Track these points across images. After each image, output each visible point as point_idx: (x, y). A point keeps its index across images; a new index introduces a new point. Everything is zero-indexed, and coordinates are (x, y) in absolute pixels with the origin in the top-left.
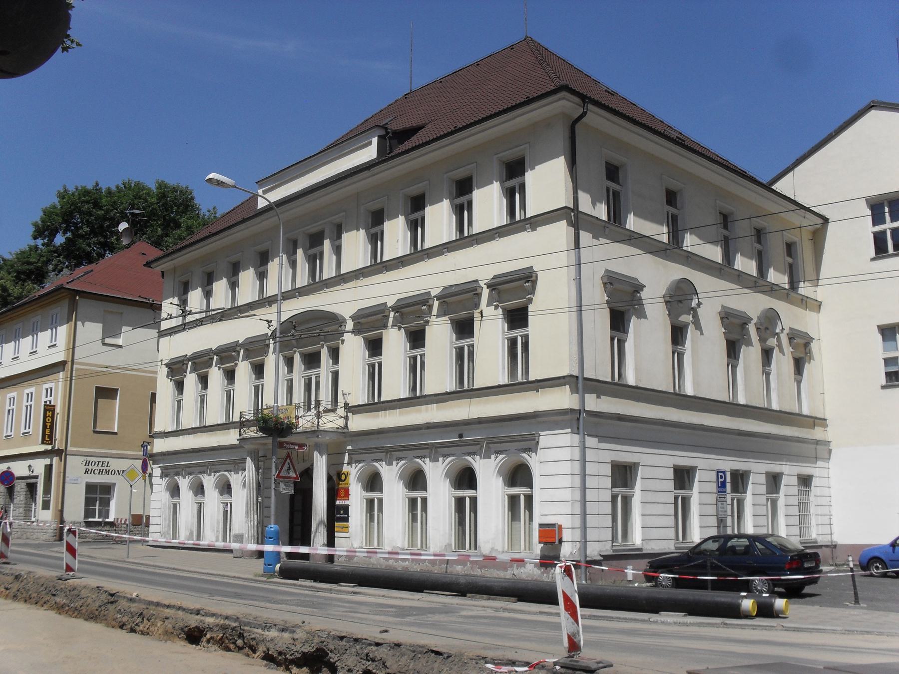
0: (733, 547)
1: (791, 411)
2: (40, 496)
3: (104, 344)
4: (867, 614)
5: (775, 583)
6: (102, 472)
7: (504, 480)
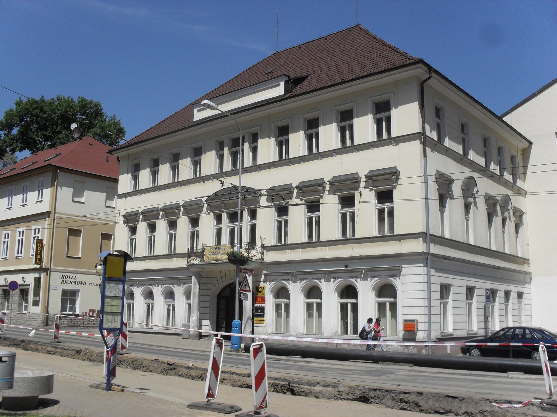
2: (31, 297)
3: (74, 201)
6: (72, 283)
7: (376, 293)
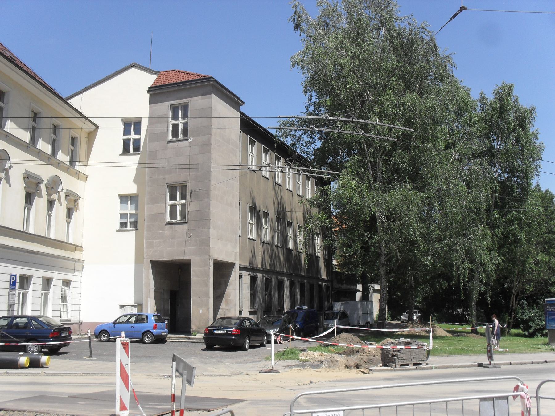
0: (17, 324)
1: (62, 240)
4: (96, 363)
5: (42, 347)
